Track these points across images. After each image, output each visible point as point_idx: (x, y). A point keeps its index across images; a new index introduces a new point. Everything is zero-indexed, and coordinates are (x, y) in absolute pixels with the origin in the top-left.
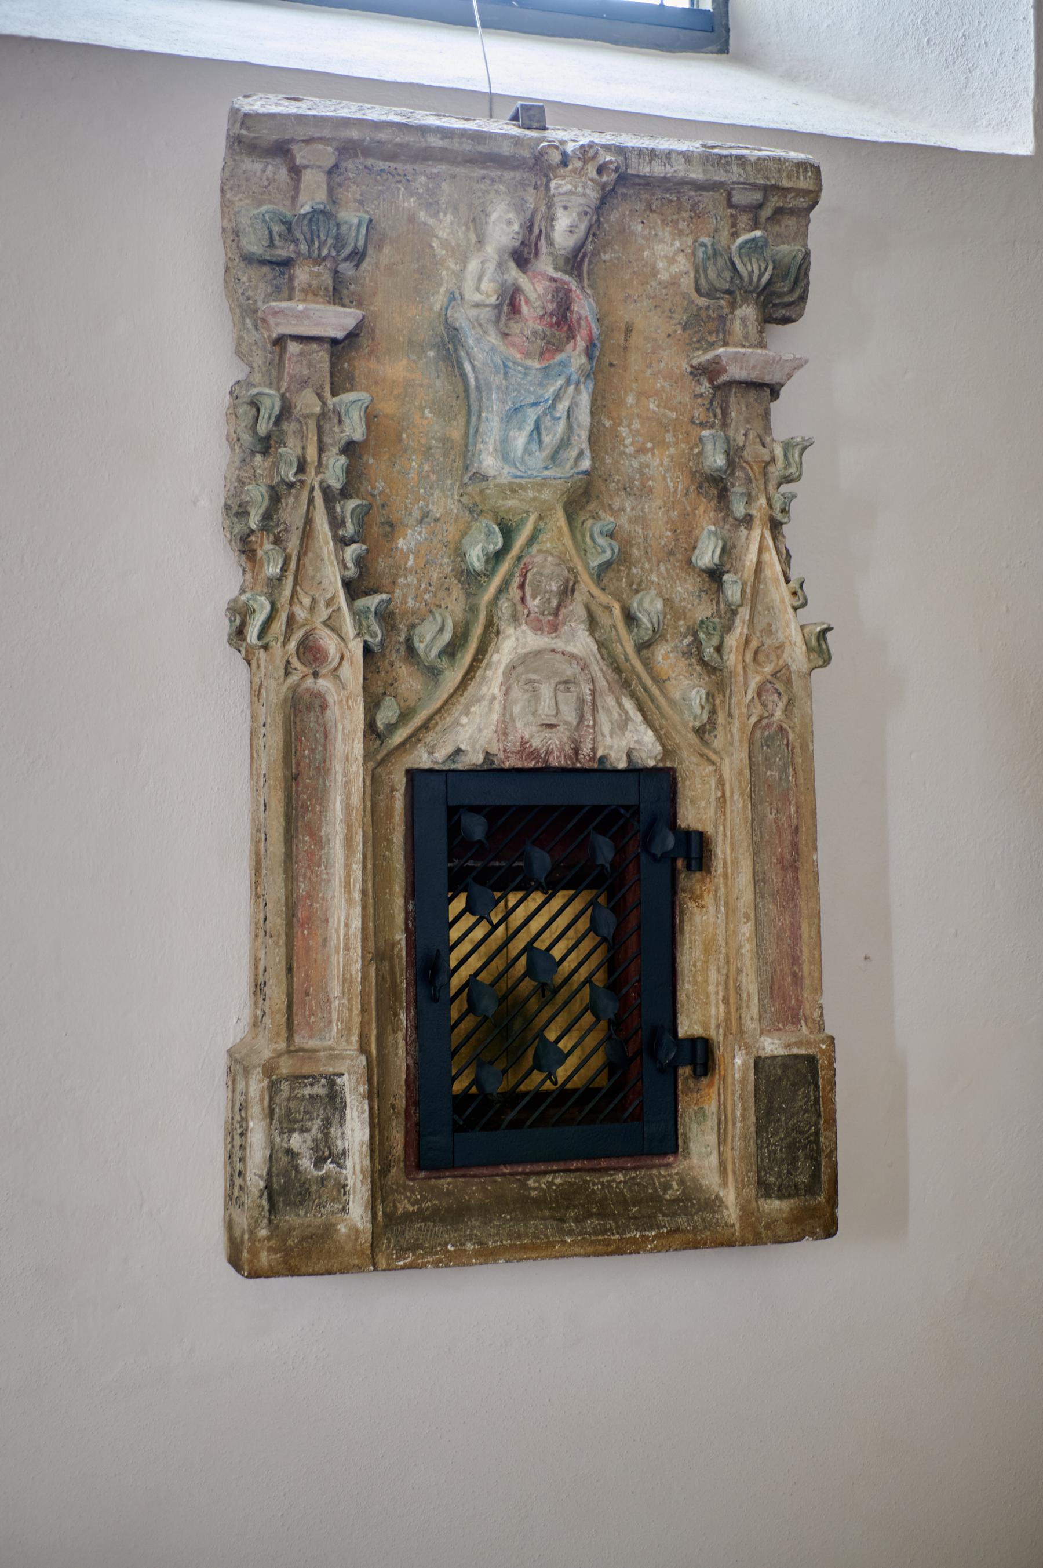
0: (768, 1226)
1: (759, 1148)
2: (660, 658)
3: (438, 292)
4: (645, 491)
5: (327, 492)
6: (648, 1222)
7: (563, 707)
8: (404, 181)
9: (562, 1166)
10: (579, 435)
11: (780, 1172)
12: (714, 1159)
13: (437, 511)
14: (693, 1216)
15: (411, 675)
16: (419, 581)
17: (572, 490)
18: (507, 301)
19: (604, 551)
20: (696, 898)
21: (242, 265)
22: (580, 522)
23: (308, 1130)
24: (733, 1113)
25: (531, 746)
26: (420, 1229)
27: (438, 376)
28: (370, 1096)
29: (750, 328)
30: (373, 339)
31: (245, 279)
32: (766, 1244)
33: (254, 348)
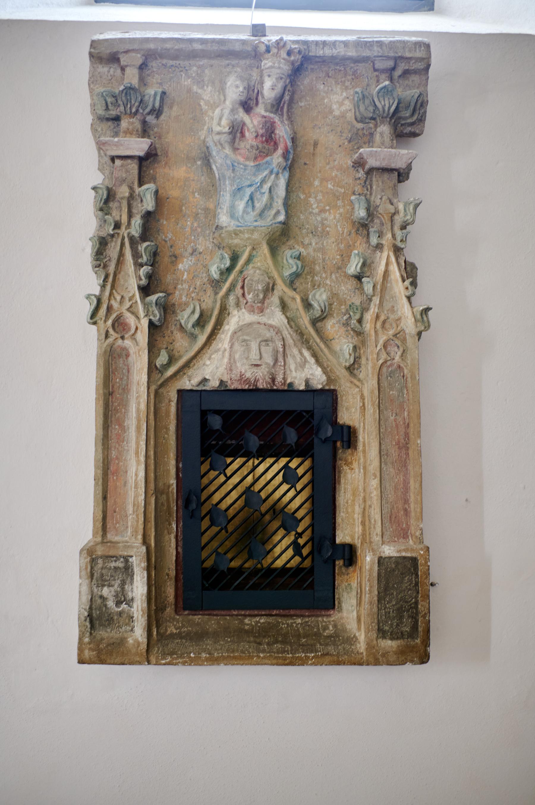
0: (383, 655)
1: (379, 609)
2: (329, 327)
3: (203, 129)
4: (325, 234)
5: (132, 239)
6: (311, 648)
7: (264, 355)
8: (184, 70)
9: (267, 612)
10: (277, 202)
11: (392, 625)
12: (355, 613)
13: (201, 248)
14: (338, 646)
15: (182, 338)
16: (190, 287)
17: (271, 233)
18: (239, 131)
19: (291, 266)
20: (348, 464)
21: (98, 122)
22: (282, 251)
23: (112, 586)
24: (365, 589)
25: (245, 376)
26: (177, 643)
27: (203, 175)
28: (148, 569)
29: (386, 138)
30: (167, 157)
31: (99, 129)
32: (382, 665)
33: (105, 166)
